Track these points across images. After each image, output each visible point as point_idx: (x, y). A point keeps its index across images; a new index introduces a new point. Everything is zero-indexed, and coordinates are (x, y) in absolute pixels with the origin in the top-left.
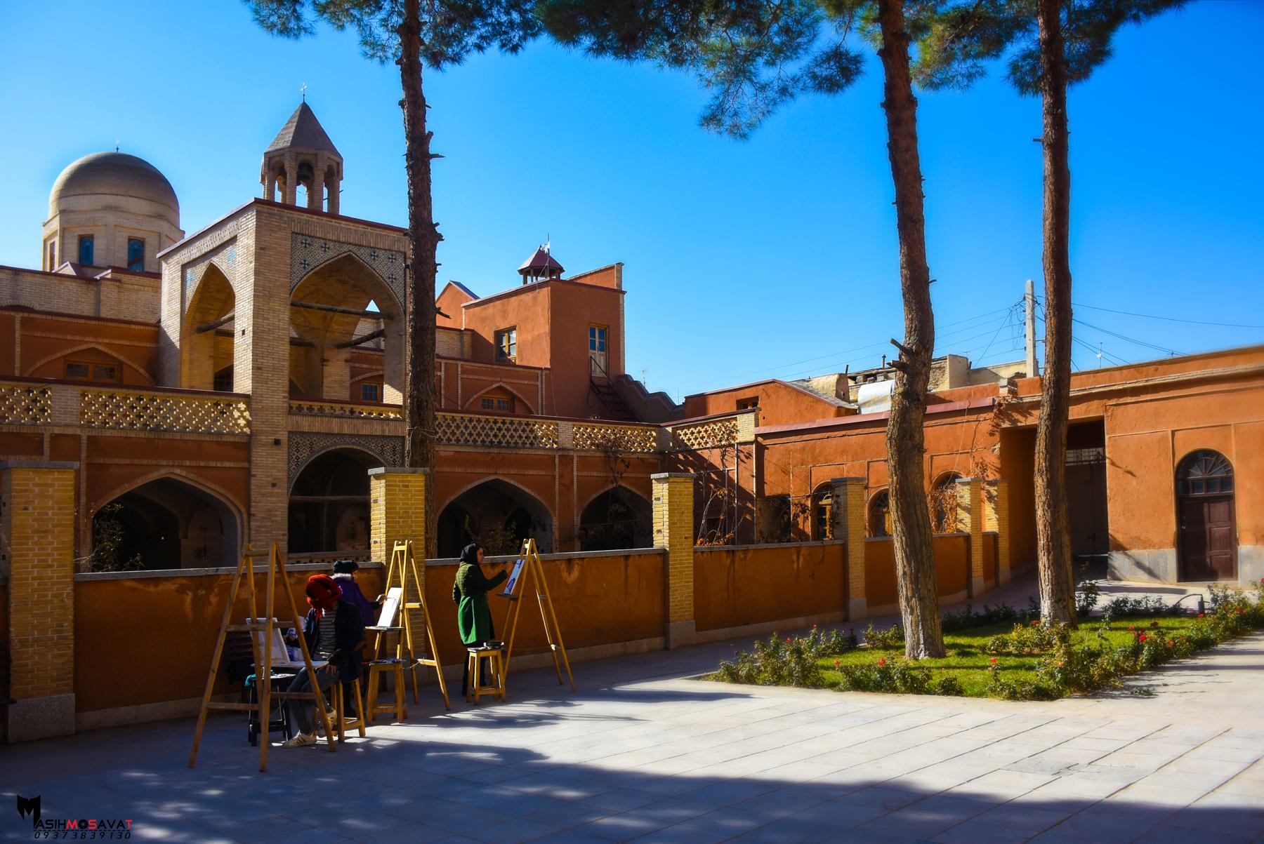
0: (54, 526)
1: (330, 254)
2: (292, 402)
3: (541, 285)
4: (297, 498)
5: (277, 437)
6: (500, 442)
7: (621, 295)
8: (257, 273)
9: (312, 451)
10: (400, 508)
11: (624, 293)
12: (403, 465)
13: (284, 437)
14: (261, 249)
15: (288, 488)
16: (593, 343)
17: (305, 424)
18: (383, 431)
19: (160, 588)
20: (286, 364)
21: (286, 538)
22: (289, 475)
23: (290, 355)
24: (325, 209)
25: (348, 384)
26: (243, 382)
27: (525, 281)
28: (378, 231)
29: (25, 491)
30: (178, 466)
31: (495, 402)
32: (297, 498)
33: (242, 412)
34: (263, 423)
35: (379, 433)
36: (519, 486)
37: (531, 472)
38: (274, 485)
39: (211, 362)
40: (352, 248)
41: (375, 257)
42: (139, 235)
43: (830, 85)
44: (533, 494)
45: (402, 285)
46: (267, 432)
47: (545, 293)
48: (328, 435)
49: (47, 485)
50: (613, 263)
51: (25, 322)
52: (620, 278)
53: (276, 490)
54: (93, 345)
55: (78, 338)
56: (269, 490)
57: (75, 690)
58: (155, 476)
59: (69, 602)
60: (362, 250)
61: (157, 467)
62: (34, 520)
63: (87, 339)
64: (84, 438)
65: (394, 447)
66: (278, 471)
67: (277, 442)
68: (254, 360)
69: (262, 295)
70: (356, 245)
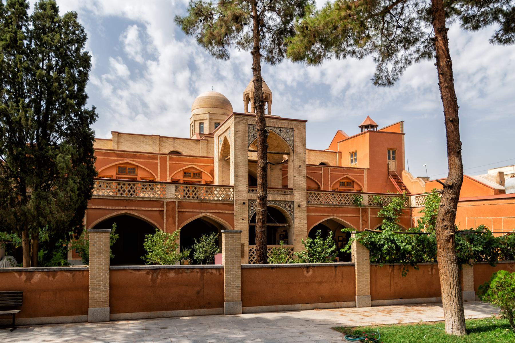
0: (103, 251)
2: (250, 188)
7: (403, 135)
10: (231, 246)
12: (87, 270)
13: (247, 202)
14: (237, 131)
15: (249, 221)
18: (285, 199)
19: (140, 272)
21: (248, 239)
22: (249, 216)
25: (281, 178)
28: (282, 121)
29: (94, 239)
30: (209, 212)
31: (346, 183)
33: (216, 196)
34: (239, 196)
36: (344, 221)
37: (349, 215)
38: (243, 219)
41: (281, 131)
42: (218, 121)
44: (350, 224)
45: (292, 142)
46: (240, 200)
50: (399, 121)
52: (402, 128)
53: (244, 221)
54: (192, 166)
55: (187, 163)
56: (241, 221)
57: (110, 306)
59: (108, 277)
60: (276, 129)
61: (202, 212)
62: (96, 249)
63: (190, 163)
64: (177, 202)
65: (290, 205)
66: (245, 214)
67: (244, 203)
70: (273, 127)
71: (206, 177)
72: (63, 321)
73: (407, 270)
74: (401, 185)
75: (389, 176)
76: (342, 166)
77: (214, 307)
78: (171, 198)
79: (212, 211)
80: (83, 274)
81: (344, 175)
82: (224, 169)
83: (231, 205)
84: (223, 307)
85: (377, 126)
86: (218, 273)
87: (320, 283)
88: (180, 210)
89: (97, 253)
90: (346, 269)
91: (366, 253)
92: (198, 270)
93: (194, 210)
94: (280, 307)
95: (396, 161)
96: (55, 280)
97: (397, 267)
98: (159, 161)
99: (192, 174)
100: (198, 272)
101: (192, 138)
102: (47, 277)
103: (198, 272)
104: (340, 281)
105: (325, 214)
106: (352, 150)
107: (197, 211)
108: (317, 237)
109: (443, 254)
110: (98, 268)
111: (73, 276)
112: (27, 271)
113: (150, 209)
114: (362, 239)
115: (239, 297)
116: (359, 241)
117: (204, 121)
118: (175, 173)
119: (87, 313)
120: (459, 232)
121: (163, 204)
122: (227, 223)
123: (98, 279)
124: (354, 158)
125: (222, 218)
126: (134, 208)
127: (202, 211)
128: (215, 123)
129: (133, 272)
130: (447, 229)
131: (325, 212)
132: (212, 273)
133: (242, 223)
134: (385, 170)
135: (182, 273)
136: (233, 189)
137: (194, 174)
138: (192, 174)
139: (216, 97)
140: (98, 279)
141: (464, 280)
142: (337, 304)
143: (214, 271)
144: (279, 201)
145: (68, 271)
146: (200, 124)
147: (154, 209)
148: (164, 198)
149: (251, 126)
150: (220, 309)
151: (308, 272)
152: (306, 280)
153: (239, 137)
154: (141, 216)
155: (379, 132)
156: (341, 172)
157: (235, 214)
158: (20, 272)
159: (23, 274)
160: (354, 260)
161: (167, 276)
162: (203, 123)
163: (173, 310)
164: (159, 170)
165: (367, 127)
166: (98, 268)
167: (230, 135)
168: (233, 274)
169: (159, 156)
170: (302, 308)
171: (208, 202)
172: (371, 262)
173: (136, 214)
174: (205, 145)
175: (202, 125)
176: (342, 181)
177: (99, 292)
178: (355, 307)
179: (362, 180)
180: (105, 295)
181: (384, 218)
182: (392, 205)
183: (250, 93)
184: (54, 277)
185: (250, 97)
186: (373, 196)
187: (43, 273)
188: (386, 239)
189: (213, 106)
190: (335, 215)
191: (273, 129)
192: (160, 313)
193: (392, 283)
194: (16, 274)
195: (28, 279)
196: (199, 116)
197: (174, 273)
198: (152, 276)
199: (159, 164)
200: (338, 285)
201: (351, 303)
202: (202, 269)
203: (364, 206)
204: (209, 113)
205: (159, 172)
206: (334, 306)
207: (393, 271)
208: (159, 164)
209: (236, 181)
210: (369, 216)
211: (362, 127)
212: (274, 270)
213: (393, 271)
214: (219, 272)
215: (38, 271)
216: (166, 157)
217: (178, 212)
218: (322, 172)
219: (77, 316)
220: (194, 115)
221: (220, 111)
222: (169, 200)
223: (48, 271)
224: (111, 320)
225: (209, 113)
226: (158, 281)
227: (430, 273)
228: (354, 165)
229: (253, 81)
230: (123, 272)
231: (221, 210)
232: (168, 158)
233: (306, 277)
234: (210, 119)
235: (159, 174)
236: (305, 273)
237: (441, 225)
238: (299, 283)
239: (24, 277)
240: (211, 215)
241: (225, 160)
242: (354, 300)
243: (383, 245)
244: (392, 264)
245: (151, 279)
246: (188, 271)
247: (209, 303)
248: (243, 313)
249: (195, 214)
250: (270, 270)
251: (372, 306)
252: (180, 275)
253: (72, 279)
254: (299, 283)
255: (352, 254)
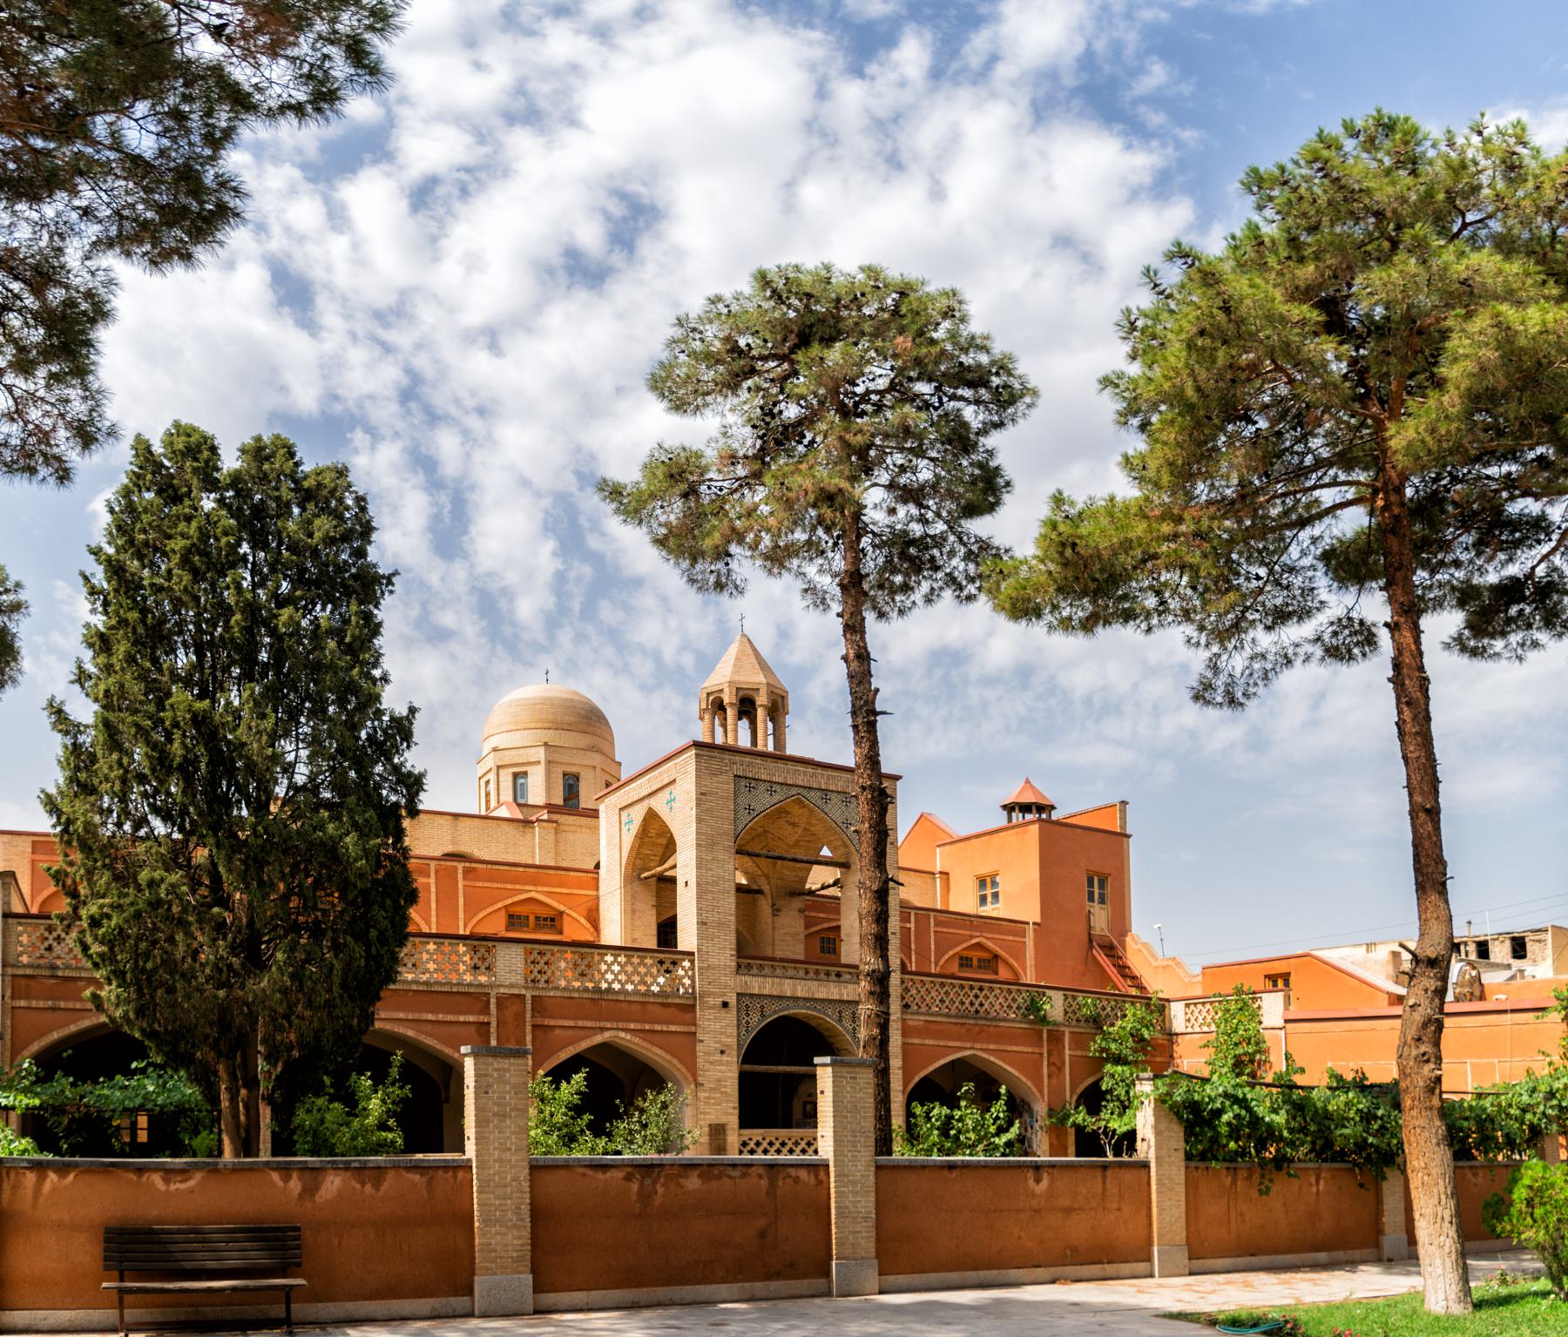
1: (776, 798)
3: (1032, 822)
4: (748, 1067)
5: (726, 999)
6: (977, 1012)
8: (699, 820)
9: (763, 1016)
11: (1129, 836)
13: (732, 1000)
16: (1091, 895)
17: (756, 985)
19: (608, 1175)
20: (733, 919)
23: (738, 904)
24: (771, 748)
26: (687, 938)
27: (1010, 820)
28: (830, 772)
30: (623, 1030)
31: (975, 962)
32: (748, 1067)
35: (836, 997)
37: (1014, 1048)
38: (722, 1052)
39: (654, 912)
40: (800, 791)
41: (826, 800)
42: (574, 770)
43: (1336, 653)
47: (1035, 828)
48: (780, 998)
49: (505, 1070)
50: (1116, 800)
51: (467, 872)
53: (725, 1058)
56: (718, 1057)
57: (533, 1271)
58: (598, 1039)
59: (526, 1184)
61: (603, 1029)
64: (528, 997)
67: (725, 1005)
68: (699, 915)
69: (705, 843)
71: (575, 929)
72: (405, 1313)
73: (1271, 1181)
74: (1124, 970)
75: (1091, 947)
76: (952, 909)
77: (804, 1277)
78: (512, 986)
79: (632, 1026)
80: (455, 1177)
81: (972, 937)
82: (638, 906)
83: (688, 1008)
84: (828, 1274)
85: (1053, 807)
86: (812, 1181)
87: (1068, 1211)
88: (539, 1021)
89: (496, 1115)
90: (1128, 1176)
91: (1177, 1133)
92: (761, 1171)
93: (580, 1023)
94: (972, 1276)
95: (1108, 906)
96: (381, 1193)
97: (1243, 1174)
98: (432, 880)
99: (532, 919)
100: (760, 1176)
101: (495, 814)
102: (358, 1186)
103: (760, 1176)
104: (1115, 1206)
105: (951, 1044)
106: (984, 870)
107: (589, 1024)
108: (963, 1103)
109: (1422, 1122)
110: (500, 1160)
111: (429, 1183)
112: (304, 1168)
113: (449, 1018)
114: (1169, 1094)
115: (872, 1250)
116: (1161, 1101)
117: (529, 769)
118: (481, 915)
119: (469, 1291)
120: (1372, 1086)
121: (488, 1003)
122: (675, 1061)
123: (500, 1191)
124: (989, 892)
125: (661, 1048)
126: (402, 1015)
127: (602, 1024)
128: (565, 775)
129: (589, 1172)
130: (1428, 1061)
131: (950, 1037)
132: (797, 1179)
133: (720, 1063)
134: (1080, 930)
135: (719, 1178)
136: (692, 962)
137: (537, 918)
138: (532, 919)
139: (567, 700)
140: (500, 1191)
141: (1385, 1207)
142: (1110, 1269)
143: (803, 1174)
144: (822, 1000)
145: (417, 1168)
146: (516, 776)
147: (462, 1018)
148: (491, 986)
149: (743, 782)
150: (820, 1283)
151: (1038, 1181)
152: (1035, 1203)
153: (710, 811)
154: (422, 1038)
155: (1057, 823)
156: (963, 928)
157: (700, 1036)
158: (285, 1170)
159: (295, 1175)
160: (1146, 1148)
161: (679, 1184)
162: (525, 774)
163: (699, 1283)
164: (433, 905)
165: (1025, 808)
166: (500, 1160)
167: (676, 805)
168: (854, 1183)
169: (433, 864)
170: (1025, 1280)
171: (622, 998)
172: (1189, 1157)
173: (410, 1033)
174: (551, 837)
175: (521, 781)
176: (965, 954)
177: (503, 1230)
178: (1151, 1276)
179: (1019, 953)
180: (520, 1238)
181: (1107, 1060)
182: (1129, 1024)
183: (727, 690)
184: (377, 1186)
185: (726, 700)
186: (1074, 998)
187: (349, 1174)
188: (1226, 1095)
189: (558, 726)
190: (978, 1046)
191: (805, 793)
192: (662, 1292)
193: (1233, 1215)
194: (275, 1176)
195: (310, 1191)
196: (514, 752)
197: (699, 1176)
198: (641, 1184)
199: (433, 889)
200: (1111, 1217)
201: (1141, 1267)
202: (771, 1166)
203: (1055, 1024)
204: (546, 744)
205: (434, 913)
206: (1101, 1274)
207: (1234, 1182)
208: (433, 889)
209: (701, 936)
210: (1067, 1052)
211: (1009, 808)
212: (955, 1173)
213: (1234, 1182)
214: (816, 1176)
215: (335, 1167)
216: (455, 868)
217: (534, 1026)
218: (912, 926)
219: (443, 1300)
220: (495, 750)
221: (583, 740)
222: (506, 991)
223: (363, 1168)
224: (536, 1312)
225: (546, 744)
226: (658, 1200)
227: (1314, 1189)
228: (989, 910)
229: (845, 658)
230: (563, 1172)
231: (659, 1023)
232: (460, 872)
233: (1033, 1195)
234: (549, 763)
235: (434, 919)
236: (1031, 1182)
237: (1414, 1052)
238: (1018, 1211)
239: (295, 1184)
240: (628, 1037)
241: (640, 879)
242: (1149, 1259)
243: (1218, 1113)
244: (1233, 1165)
245: (639, 1194)
246: (736, 1173)
247: (792, 1265)
248: (881, 1292)
249: (582, 1033)
250: (946, 1172)
251: (1191, 1274)
252: (714, 1184)
253: (425, 1193)
254: (1018, 1211)
255: (1139, 1137)
